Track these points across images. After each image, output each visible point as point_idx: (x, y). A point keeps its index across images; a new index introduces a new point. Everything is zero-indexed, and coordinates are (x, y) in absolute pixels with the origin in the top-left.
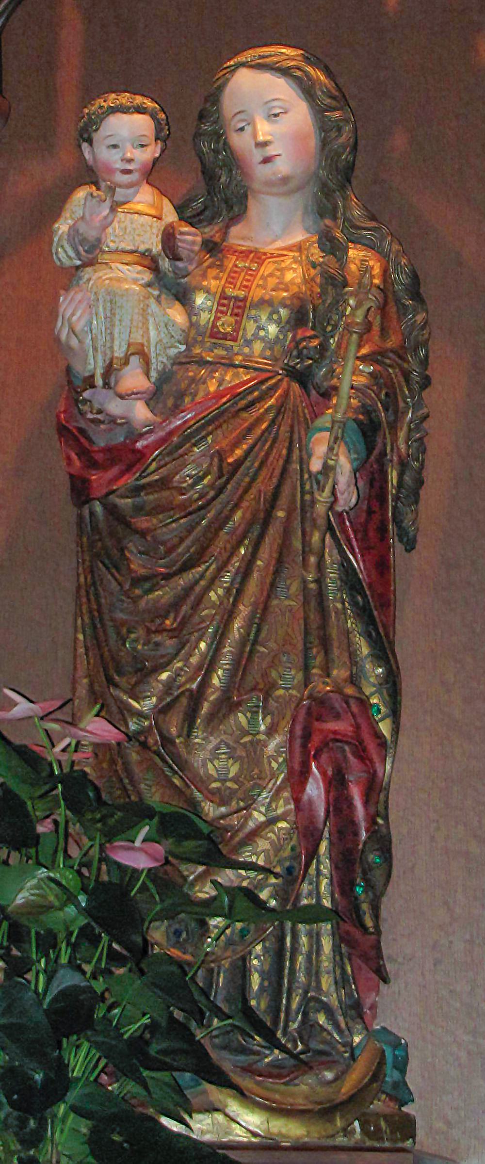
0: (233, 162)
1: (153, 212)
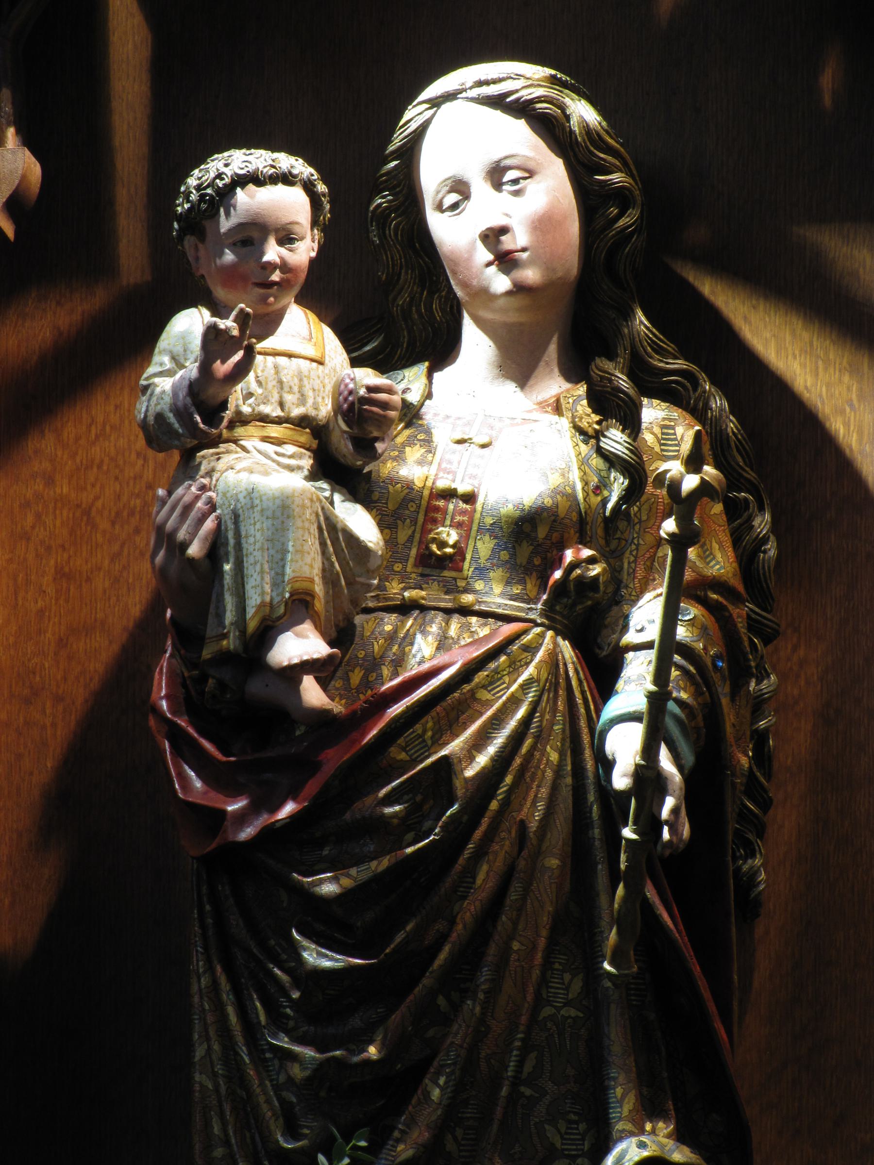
1: (311, 352)
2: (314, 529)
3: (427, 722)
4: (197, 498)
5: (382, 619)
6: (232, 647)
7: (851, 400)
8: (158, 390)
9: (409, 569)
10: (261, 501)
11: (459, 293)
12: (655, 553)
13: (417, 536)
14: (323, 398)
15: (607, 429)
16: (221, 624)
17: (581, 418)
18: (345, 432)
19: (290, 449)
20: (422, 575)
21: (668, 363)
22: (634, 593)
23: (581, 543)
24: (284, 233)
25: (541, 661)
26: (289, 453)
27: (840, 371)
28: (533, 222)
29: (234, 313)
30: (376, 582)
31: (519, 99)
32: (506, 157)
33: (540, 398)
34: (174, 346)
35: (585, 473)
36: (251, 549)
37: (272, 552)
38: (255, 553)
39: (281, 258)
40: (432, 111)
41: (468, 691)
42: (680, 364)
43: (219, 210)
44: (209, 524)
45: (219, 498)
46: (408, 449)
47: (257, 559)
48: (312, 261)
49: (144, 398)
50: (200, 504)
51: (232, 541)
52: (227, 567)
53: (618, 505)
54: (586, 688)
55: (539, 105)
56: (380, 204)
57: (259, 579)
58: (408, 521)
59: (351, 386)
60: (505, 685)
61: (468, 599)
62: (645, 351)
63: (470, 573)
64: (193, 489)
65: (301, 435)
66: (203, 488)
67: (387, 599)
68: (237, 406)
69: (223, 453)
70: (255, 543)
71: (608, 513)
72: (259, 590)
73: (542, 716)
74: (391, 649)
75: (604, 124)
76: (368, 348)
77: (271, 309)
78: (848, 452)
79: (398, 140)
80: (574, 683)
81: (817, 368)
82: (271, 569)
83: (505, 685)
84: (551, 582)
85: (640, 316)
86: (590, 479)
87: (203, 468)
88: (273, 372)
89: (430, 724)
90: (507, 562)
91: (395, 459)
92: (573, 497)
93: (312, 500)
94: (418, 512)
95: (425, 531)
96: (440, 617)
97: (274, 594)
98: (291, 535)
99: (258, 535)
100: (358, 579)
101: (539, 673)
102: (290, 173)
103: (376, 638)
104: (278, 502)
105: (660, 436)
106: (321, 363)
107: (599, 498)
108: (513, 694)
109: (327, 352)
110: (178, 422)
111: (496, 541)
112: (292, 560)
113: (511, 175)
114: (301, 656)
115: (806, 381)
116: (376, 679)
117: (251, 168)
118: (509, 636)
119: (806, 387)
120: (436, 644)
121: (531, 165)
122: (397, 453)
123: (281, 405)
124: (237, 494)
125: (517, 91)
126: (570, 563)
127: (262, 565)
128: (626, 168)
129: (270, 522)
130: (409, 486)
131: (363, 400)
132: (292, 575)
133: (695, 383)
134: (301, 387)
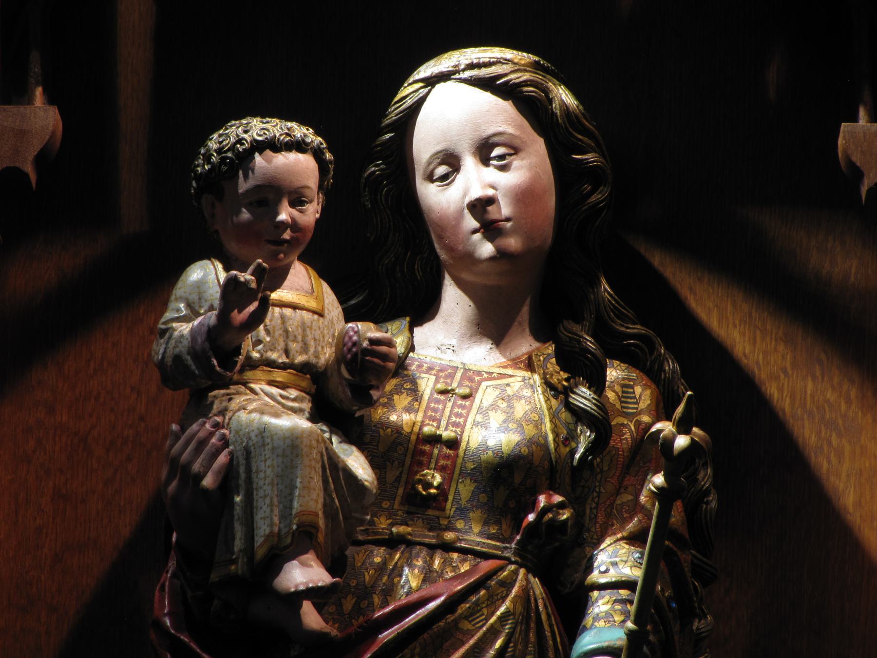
0: (291, 151)
1: (312, 304)
2: (319, 467)
3: (415, 648)
4: (211, 434)
5: (372, 552)
6: (240, 572)
7: (786, 368)
8: (176, 334)
9: (395, 507)
10: (272, 440)
11: (443, 255)
12: (614, 501)
13: (404, 477)
14: (323, 347)
15: (576, 386)
16: (230, 549)
17: (552, 375)
18: (346, 379)
19: (293, 393)
20: (408, 513)
21: (628, 328)
22: (595, 537)
23: (550, 489)
24: (296, 196)
25: (515, 596)
26: (292, 397)
27: (776, 340)
28: (517, 195)
29: (252, 268)
30: (368, 517)
31: (507, 82)
32: (494, 135)
33: (513, 355)
34: (190, 294)
35: (556, 426)
36: (261, 483)
37: (281, 487)
38: (265, 487)
39: (293, 219)
40: (426, 90)
41: (452, 621)
42: (637, 329)
43: (238, 173)
44: (222, 459)
45: (232, 435)
46: (396, 397)
47: (266, 492)
48: (318, 221)
49: (162, 341)
50: (214, 440)
51: (243, 476)
52: (238, 499)
53: (584, 455)
54: (554, 622)
55: (526, 89)
56: (375, 171)
57: (268, 510)
58: (396, 462)
59: (355, 338)
60: (484, 617)
61: (450, 536)
62: (609, 316)
63: (452, 513)
64: (208, 426)
65: (303, 380)
66: (217, 426)
67: (376, 533)
68: (248, 352)
69: (234, 394)
70: (265, 478)
71: (575, 463)
72: (268, 522)
73: (515, 646)
74: (381, 580)
75: (581, 107)
76: (353, 302)
77: (280, 264)
78: (781, 414)
79: (394, 112)
80: (544, 617)
81: (755, 337)
82: (280, 503)
83: (484, 617)
84: (524, 524)
85: (605, 285)
86: (560, 431)
87: (215, 407)
88: (279, 321)
89: (418, 650)
90: (485, 504)
91: (384, 405)
92: (546, 446)
93: (318, 441)
94: (406, 455)
95: (412, 473)
96: (424, 552)
97: (282, 526)
98: (299, 473)
99: (269, 471)
100: (354, 514)
101: (515, 606)
102: (303, 141)
103: (367, 569)
104: (288, 442)
105: (620, 394)
106: (321, 315)
107: (568, 449)
108: (492, 625)
109: (326, 305)
110: (195, 364)
111: (476, 484)
112: (299, 495)
113: (497, 151)
114: (307, 583)
115: (744, 348)
116: (368, 607)
117: (269, 135)
118: (488, 572)
119: (745, 355)
120: (421, 577)
121: (517, 143)
122: (386, 400)
123: (287, 352)
124: (249, 433)
125: (506, 75)
126: (544, 507)
127: (271, 499)
128: (598, 149)
129: (280, 459)
130: (397, 429)
131: (365, 352)
132: (300, 509)
133: (652, 347)
134: (304, 336)
